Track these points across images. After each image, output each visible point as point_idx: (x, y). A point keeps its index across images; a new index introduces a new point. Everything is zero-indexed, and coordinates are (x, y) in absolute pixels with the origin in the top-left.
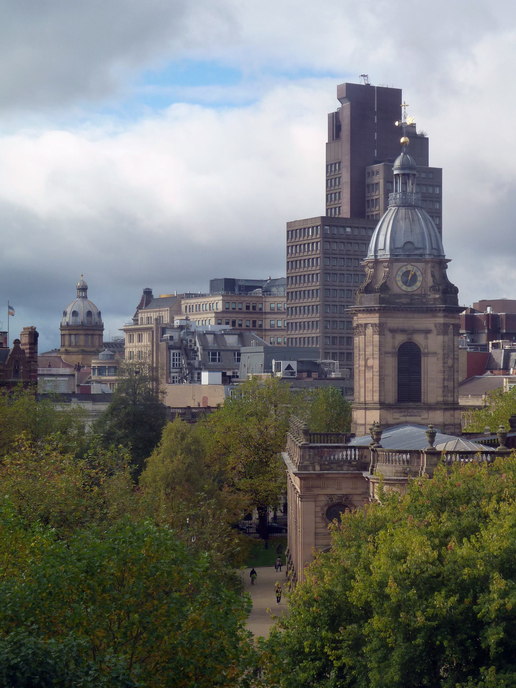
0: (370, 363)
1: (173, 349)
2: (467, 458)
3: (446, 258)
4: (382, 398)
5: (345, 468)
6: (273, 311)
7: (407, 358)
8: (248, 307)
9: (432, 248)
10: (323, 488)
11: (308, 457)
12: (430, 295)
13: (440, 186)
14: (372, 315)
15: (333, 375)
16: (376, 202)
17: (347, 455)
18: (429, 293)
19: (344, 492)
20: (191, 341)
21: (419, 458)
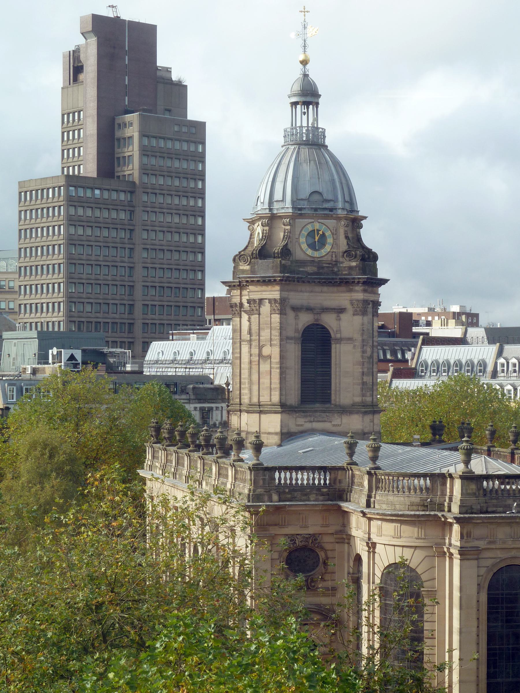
0: (266, 351)
2: (508, 483)
3: (360, 214)
4: (283, 397)
5: (312, 497)
6: (12, 290)
7: (313, 345)
9: (345, 201)
10: (282, 526)
11: (261, 482)
12: (342, 263)
13: (203, 143)
14: (270, 288)
15: (129, 368)
16: (129, 159)
18: (341, 259)
19: (311, 531)
21: (444, 484)
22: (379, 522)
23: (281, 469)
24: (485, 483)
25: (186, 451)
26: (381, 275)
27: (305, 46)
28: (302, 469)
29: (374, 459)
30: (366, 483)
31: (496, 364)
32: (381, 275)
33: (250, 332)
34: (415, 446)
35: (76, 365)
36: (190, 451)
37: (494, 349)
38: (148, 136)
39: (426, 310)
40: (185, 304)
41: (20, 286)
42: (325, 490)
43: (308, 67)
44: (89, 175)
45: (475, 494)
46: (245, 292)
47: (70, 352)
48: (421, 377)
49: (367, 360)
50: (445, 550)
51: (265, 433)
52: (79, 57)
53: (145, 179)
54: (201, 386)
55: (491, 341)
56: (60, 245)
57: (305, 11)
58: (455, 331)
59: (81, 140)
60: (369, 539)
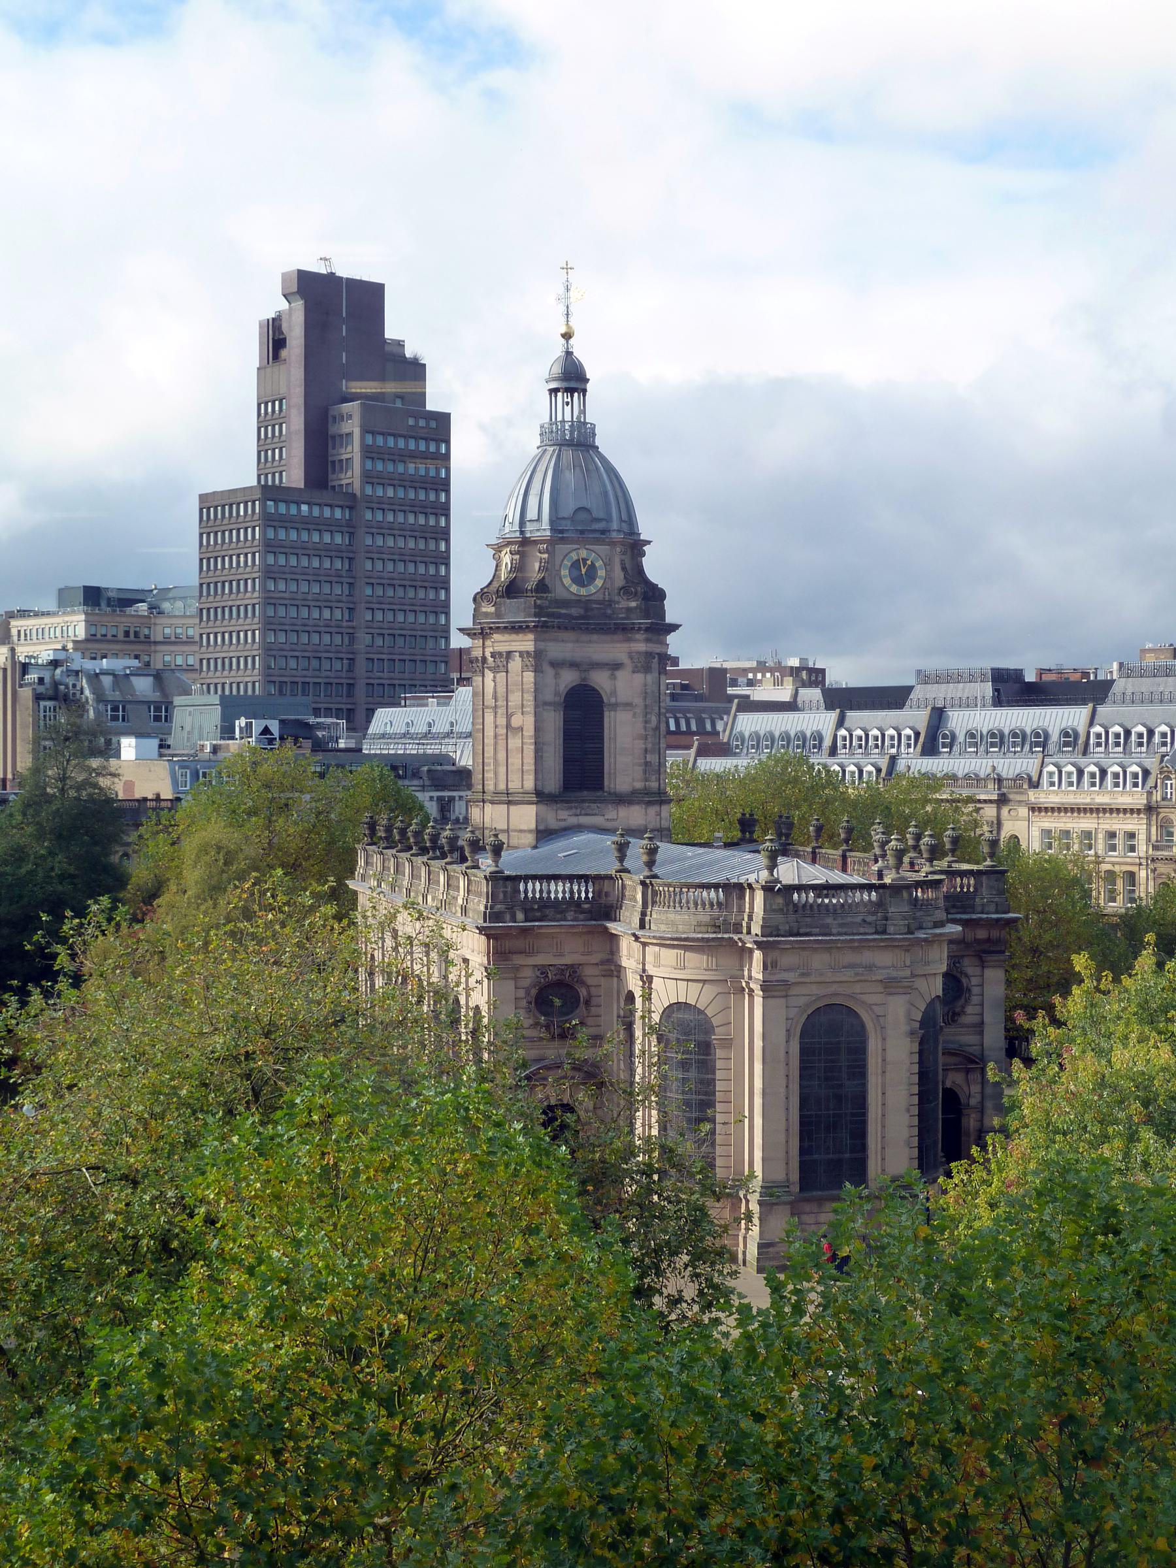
0: (516, 721)
1: (44, 699)
2: (827, 896)
3: (642, 537)
4: (539, 783)
5: (570, 915)
8: (127, 634)
9: (621, 521)
11: (501, 896)
12: (618, 602)
13: (448, 442)
15: (342, 744)
17: (564, 892)
18: (616, 598)
19: (567, 960)
20: (74, 686)
21: (742, 897)
22: (657, 948)
23: (526, 878)
24: (796, 896)
25: (407, 855)
26: (670, 618)
27: (567, 315)
28: (556, 878)
29: (650, 864)
30: (639, 897)
31: (835, 736)
32: (670, 618)
33: (495, 698)
34: (717, 847)
35: (271, 741)
36: (412, 855)
37: (833, 716)
38: (373, 433)
39: (754, 664)
40: (402, 657)
41: (201, 635)
42: (586, 906)
43: (571, 341)
44: (294, 486)
45: (782, 910)
46: (488, 643)
47: (263, 723)
48: (735, 754)
49: (651, 733)
50: (744, 984)
51: (515, 831)
52: (280, 327)
53: (369, 490)
54: (439, 768)
55: (829, 707)
56: (254, 579)
57: (567, 268)
58: (784, 694)
59: (283, 438)
60: (644, 970)
